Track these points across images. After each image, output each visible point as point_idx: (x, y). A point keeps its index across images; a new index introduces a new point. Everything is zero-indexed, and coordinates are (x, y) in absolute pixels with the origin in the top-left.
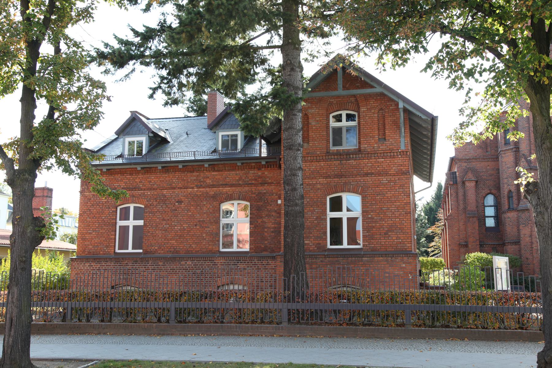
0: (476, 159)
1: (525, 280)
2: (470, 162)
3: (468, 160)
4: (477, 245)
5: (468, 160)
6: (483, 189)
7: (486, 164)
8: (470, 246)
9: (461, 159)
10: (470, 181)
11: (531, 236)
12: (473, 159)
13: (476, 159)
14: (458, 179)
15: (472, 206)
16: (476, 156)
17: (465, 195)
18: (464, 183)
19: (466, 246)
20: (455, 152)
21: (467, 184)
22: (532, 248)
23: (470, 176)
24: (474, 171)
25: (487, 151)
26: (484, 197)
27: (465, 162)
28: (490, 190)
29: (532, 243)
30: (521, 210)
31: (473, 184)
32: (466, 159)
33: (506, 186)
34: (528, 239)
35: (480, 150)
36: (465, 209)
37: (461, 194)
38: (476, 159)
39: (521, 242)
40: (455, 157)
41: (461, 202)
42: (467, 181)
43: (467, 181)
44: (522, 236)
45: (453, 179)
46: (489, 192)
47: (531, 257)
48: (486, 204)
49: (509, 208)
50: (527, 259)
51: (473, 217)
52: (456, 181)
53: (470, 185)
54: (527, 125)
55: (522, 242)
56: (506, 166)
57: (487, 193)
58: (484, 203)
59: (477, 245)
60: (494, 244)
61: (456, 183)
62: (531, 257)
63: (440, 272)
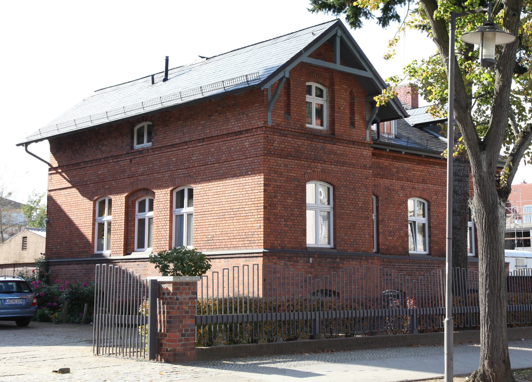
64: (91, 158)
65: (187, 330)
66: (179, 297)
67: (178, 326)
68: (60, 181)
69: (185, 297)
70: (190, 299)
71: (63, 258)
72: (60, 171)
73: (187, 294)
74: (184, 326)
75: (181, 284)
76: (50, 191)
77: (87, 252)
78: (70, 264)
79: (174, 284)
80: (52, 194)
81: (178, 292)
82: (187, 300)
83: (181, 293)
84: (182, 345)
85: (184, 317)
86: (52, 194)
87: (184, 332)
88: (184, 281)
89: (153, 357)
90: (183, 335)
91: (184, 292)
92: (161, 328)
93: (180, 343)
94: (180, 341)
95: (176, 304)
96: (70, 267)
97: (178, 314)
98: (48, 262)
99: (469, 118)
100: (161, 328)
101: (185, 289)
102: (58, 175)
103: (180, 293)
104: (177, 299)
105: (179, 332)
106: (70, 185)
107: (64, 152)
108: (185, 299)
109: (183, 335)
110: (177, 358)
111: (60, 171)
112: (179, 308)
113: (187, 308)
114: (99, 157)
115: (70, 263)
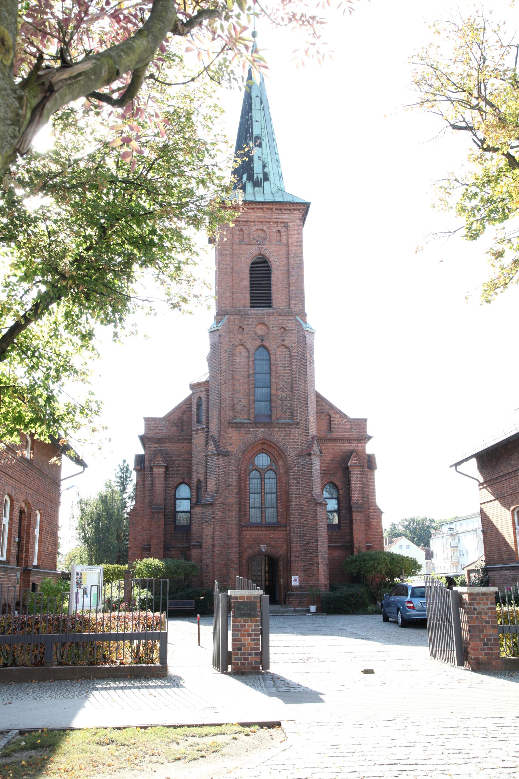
0: (168, 439)
1: (502, 597)
2: (162, 443)
3: (159, 439)
4: (161, 548)
5: (159, 440)
6: (174, 477)
7: (181, 445)
8: (152, 549)
9: (151, 439)
10: (159, 466)
11: (213, 537)
12: (165, 439)
13: (169, 439)
14: (147, 463)
15: (159, 499)
16: (169, 436)
17: (152, 485)
18: (151, 468)
19: (149, 549)
20: (145, 429)
21: (155, 470)
22: (213, 552)
23: (159, 460)
24: (163, 453)
25: (182, 430)
26: (176, 488)
27: (156, 442)
28: (183, 478)
29: (213, 546)
30: (205, 504)
31: (162, 470)
32: (157, 439)
33: (195, 474)
34: (210, 541)
35: (175, 428)
36: (151, 501)
37: (147, 483)
38: (169, 439)
39: (203, 544)
40: (144, 435)
41: (148, 493)
42: (156, 466)
43: (156, 466)
44: (204, 537)
45: (141, 462)
46: (181, 480)
47: (212, 564)
48: (177, 497)
49: (197, 502)
50: (207, 565)
51: (159, 512)
52: (144, 466)
53: (159, 471)
54: (218, 401)
55: (204, 545)
56: (197, 449)
57: (179, 482)
58: (175, 495)
59: (161, 548)
60: (183, 548)
61: (144, 469)
62: (212, 564)
63: (114, 584)
64: (505, 473)
65: (489, 640)
66: (476, 607)
67: (479, 635)
68: (487, 495)
69: (484, 607)
70: (489, 609)
71: (497, 564)
72: (485, 486)
73: (485, 604)
74: (485, 635)
75: (478, 594)
76: (481, 504)
77: (512, 559)
78: (502, 570)
79: (470, 594)
80: (483, 506)
81: (475, 602)
82: (486, 610)
83: (478, 604)
84: (485, 654)
85: (485, 627)
86: (483, 506)
87: (486, 641)
88: (479, 591)
89: (461, 664)
90: (485, 644)
91: (482, 602)
92: (465, 635)
93: (483, 652)
94: (483, 649)
95: (474, 613)
96: (502, 573)
97: (477, 624)
98: (487, 568)
99: (147, 447)
100: (465, 635)
101: (483, 599)
102: (485, 490)
103: (477, 603)
104: (475, 609)
105: (480, 640)
106: (493, 498)
107: (486, 469)
108: (484, 609)
109: (485, 644)
110: (481, 666)
111: (485, 486)
112: (477, 618)
113: (487, 618)
114: (510, 471)
115: (501, 569)
